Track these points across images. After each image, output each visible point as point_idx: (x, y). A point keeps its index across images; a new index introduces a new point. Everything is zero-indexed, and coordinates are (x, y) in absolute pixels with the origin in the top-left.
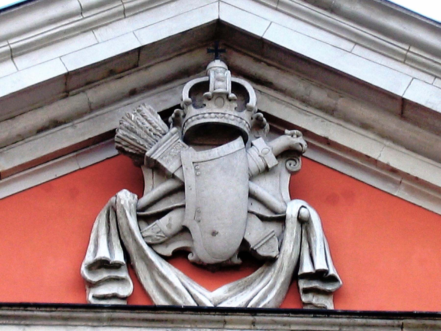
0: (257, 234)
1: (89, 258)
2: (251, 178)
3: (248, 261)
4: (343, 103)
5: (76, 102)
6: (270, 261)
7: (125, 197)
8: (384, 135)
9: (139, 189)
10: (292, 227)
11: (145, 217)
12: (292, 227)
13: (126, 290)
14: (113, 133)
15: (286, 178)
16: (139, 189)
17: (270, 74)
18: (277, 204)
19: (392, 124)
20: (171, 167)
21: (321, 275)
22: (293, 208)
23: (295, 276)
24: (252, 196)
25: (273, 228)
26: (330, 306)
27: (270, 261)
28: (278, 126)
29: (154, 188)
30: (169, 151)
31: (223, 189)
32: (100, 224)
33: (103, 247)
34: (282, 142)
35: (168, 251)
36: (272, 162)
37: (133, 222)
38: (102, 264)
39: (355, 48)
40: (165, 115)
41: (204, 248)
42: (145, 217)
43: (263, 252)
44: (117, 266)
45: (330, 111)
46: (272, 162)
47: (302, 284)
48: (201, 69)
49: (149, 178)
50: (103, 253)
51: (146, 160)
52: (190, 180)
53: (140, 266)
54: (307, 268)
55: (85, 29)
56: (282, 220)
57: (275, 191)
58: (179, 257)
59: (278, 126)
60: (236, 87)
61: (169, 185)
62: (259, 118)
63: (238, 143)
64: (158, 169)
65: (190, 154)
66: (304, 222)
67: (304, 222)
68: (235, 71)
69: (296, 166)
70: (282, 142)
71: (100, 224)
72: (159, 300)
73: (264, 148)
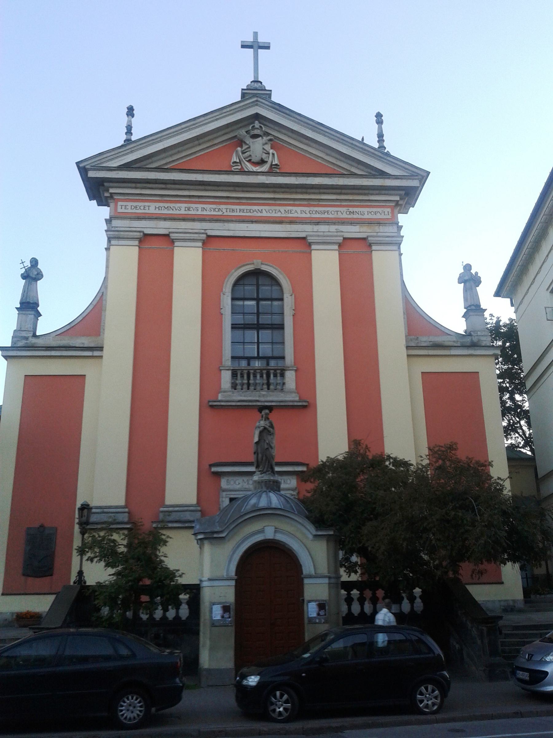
0: (264, 156)
1: (232, 161)
2: (264, 145)
3: (262, 162)
4: (281, 130)
5: (229, 129)
6: (267, 162)
7: (239, 149)
8: (289, 136)
9: (242, 147)
10: (271, 155)
11: (243, 153)
12: (271, 155)
13: (239, 167)
14: (236, 136)
15: (270, 145)
16: (242, 147)
17: (267, 124)
18: (268, 150)
19: (290, 134)
20: (248, 142)
21: (276, 165)
22: (271, 151)
23: (272, 165)
24: (263, 149)
25: (267, 155)
26: (278, 171)
27: (267, 162)
28: (268, 134)
29: (245, 147)
30: (249, 141)
31: (257, 147)
32: (234, 155)
33: (235, 159)
34: (269, 137)
35: (247, 159)
36: (267, 142)
37: (241, 154)
38: (235, 162)
39: (227, 372)
40: (246, 132)
41: (254, 159)
42: (243, 153)
43: (266, 160)
44: (238, 163)
45: (279, 132)
46: (267, 142)
47: (273, 166)
48: (254, 123)
49: (244, 145)
50: (235, 160)
51: (69, 627)
52: (251, 144)
53: (242, 163)
54: (274, 163)
55: (231, 114)
56: (269, 154)
57: (268, 147)
58: (249, 161)
59: (268, 134)
60: (261, 127)
61: (247, 146)
62: (25, 275)
63: (260, 138)
64: (245, 143)
65: (251, 140)
66: (273, 154)
67: (273, 154)
68: (260, 123)
69: (272, 142)
70: (269, 137)
71: (234, 155)
72: (246, 170)
73: (265, 138)
